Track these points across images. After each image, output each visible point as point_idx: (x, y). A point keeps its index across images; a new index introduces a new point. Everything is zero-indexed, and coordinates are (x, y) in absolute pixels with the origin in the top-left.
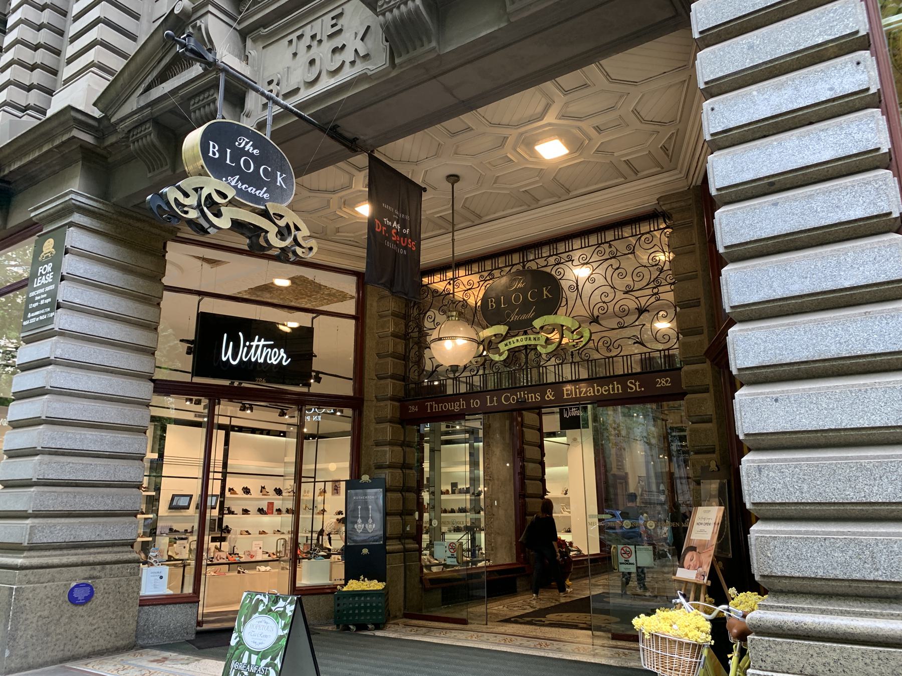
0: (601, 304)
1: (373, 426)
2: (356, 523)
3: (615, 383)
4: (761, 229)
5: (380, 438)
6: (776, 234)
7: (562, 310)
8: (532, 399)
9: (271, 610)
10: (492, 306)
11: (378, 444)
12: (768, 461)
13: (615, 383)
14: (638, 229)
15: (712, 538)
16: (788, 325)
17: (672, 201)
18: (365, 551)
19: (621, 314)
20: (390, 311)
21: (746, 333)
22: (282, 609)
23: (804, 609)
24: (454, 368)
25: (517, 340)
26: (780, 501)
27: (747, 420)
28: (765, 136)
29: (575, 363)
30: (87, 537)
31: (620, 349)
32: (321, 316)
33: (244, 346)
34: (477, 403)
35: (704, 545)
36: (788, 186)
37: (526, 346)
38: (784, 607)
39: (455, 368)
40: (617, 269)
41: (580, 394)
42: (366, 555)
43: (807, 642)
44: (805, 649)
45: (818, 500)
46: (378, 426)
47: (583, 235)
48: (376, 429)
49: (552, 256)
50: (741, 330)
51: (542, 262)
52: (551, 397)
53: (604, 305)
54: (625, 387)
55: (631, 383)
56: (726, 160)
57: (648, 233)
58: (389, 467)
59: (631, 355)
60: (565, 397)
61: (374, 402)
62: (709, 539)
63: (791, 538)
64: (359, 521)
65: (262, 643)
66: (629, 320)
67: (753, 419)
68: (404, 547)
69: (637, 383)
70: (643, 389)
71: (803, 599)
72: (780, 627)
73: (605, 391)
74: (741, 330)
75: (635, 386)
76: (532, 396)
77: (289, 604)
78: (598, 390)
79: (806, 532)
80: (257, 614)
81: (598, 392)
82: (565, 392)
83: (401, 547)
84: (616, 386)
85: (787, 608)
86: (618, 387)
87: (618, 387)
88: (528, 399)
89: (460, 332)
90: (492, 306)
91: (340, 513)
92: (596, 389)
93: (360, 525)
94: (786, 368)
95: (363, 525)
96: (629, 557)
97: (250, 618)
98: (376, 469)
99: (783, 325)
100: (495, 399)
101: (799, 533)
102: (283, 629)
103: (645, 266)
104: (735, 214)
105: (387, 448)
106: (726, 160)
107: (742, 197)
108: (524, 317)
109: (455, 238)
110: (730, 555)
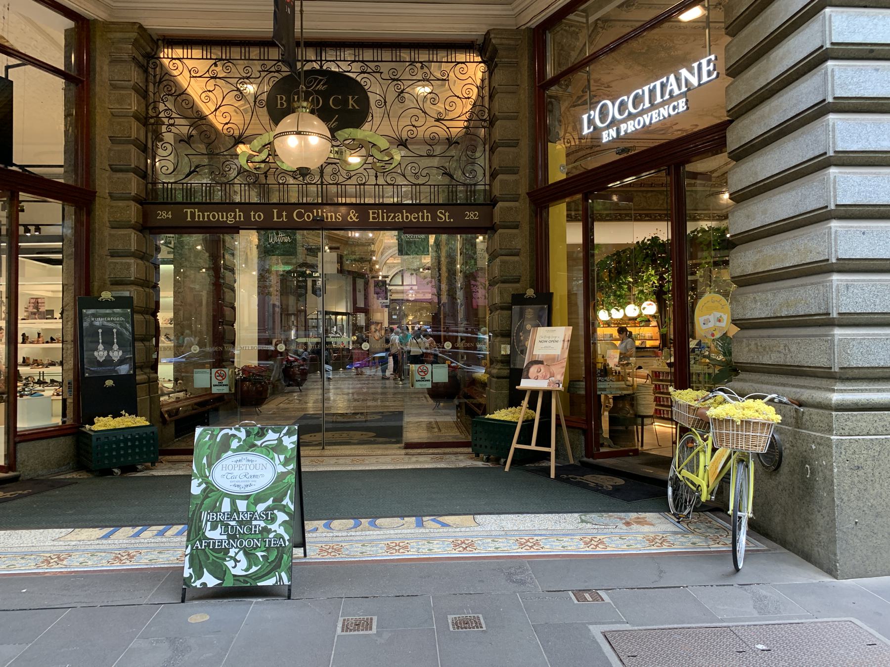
0: (412, 128)
1: (107, 232)
2: (96, 349)
3: (425, 211)
4: (865, 89)
5: (120, 247)
6: (875, 95)
7: (367, 126)
9: (255, 445)
10: (282, 104)
11: (114, 254)
12: (852, 281)
13: (425, 211)
15: (562, 352)
16: (875, 174)
17: (503, 36)
18: (109, 383)
19: (431, 142)
20: (132, 83)
21: (846, 175)
23: (866, 390)
24: (303, 172)
26: (860, 311)
27: (841, 248)
28: (865, 7)
29: (379, 185)
31: (428, 177)
32: (29, 68)
34: (259, 216)
35: (553, 359)
36: (881, 57)
38: (854, 390)
39: (305, 172)
40: (209, 91)
41: (387, 219)
42: (111, 388)
43: (873, 412)
44: (871, 417)
45: (885, 311)
46: (113, 232)
47: (224, 45)
48: (110, 235)
49: (357, 61)
50: (840, 173)
51: (344, 67)
52: (354, 219)
53: (414, 129)
54: (435, 216)
55: (441, 213)
56: (842, 18)
57: (333, 61)
58: (132, 283)
60: (371, 220)
61: (109, 200)
62: (559, 353)
63: (865, 339)
64: (101, 347)
65: (251, 485)
66: (438, 150)
67: (846, 247)
68: (149, 377)
69: (447, 214)
70: (452, 220)
71: (861, 383)
72: (856, 404)
73: (415, 218)
74: (840, 173)
77: (285, 435)
78: (407, 217)
79: (874, 335)
80: (230, 453)
82: (371, 216)
83: (145, 377)
84: (425, 215)
85: (856, 390)
86: (428, 216)
87: (428, 216)
89: (313, 125)
90: (282, 104)
91: (617, 309)
92: (405, 215)
93: (101, 353)
94: (870, 208)
95: (106, 353)
96: (426, 374)
98: (112, 284)
99: (871, 173)
100: (284, 213)
101: (869, 335)
102: (285, 464)
103: (458, 97)
104: (845, 69)
105: (131, 261)
106: (842, 18)
107: (846, 56)
109: (304, 9)
110: (672, 360)
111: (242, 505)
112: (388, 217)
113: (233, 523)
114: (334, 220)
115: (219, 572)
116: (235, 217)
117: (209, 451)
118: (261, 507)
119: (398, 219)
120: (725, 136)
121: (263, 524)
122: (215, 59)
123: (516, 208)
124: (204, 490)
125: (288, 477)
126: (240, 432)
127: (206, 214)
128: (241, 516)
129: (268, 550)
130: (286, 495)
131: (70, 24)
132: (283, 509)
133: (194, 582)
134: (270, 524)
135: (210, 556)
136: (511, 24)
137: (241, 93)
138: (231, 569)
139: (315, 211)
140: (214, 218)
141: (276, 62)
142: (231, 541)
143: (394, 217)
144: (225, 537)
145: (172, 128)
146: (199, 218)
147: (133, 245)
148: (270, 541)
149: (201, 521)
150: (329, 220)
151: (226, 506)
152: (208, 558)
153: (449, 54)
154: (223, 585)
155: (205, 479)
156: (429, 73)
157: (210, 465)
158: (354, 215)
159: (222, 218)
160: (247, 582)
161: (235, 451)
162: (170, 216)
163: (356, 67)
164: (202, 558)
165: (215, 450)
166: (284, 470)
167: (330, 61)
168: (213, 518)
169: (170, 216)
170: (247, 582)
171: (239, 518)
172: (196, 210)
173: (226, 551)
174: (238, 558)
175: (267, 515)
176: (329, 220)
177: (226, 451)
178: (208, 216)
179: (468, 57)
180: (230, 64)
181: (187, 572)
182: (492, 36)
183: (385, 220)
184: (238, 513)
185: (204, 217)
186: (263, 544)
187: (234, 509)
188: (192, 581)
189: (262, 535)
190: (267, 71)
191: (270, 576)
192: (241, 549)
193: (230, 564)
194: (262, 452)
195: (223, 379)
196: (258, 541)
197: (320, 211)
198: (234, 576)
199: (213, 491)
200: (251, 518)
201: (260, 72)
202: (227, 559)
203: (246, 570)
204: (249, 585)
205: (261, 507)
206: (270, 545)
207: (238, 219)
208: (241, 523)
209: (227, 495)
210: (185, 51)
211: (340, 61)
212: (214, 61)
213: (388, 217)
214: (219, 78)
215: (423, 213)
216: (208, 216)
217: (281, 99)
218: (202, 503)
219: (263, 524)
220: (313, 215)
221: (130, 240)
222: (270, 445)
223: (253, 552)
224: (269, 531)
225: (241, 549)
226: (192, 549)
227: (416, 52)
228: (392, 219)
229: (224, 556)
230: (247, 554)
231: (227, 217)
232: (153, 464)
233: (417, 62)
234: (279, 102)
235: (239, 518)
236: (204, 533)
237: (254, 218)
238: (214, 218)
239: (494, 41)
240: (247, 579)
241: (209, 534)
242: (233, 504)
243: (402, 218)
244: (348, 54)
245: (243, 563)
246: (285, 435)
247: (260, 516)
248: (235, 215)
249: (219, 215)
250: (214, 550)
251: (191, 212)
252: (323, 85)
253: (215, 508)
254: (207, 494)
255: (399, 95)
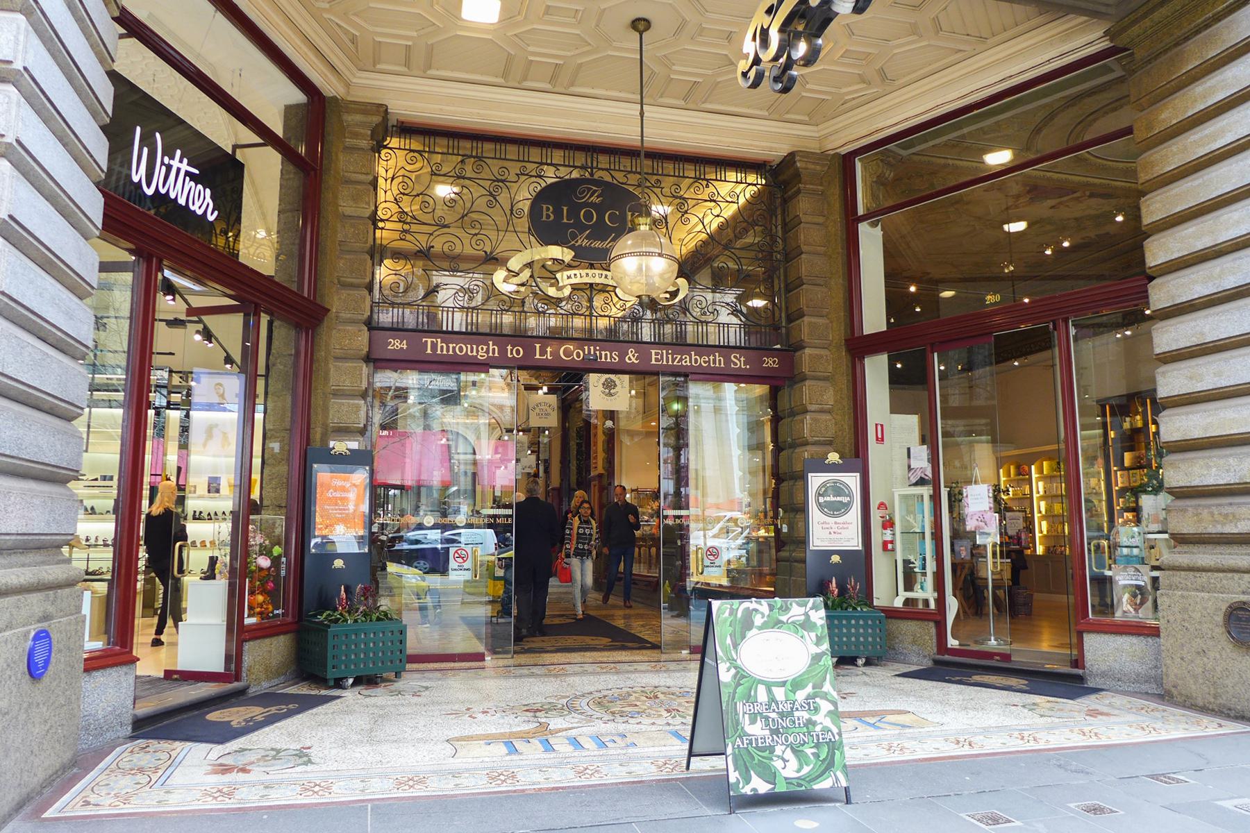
3: (717, 354)
8: (606, 358)
10: (548, 216)
13: (717, 354)
14: (723, 175)
22: (803, 618)
25: (587, 274)
30: (1240, 479)
33: (162, 163)
37: (591, 285)
41: (673, 362)
49: (634, 173)
51: (620, 176)
52: (634, 360)
54: (728, 361)
55: (735, 357)
57: (607, 170)
59: (728, 324)
60: (653, 362)
69: (742, 359)
70: (748, 367)
73: (705, 362)
75: (740, 361)
76: (606, 355)
77: (811, 609)
78: (696, 361)
80: (754, 631)
81: (696, 362)
82: (654, 357)
84: (717, 359)
88: (601, 358)
90: (548, 216)
92: (693, 358)
97: (743, 637)
102: (818, 643)
108: (597, 244)
111: (779, 693)
112: (673, 360)
113: (774, 715)
114: (609, 360)
115: (770, 777)
116: (487, 352)
117: (731, 629)
118: (801, 695)
119: (686, 362)
120: (1147, 291)
121: (806, 715)
122: (463, 156)
123: (827, 356)
124: (735, 676)
125: (824, 658)
126: (762, 605)
127: (451, 346)
128: (781, 706)
129: (817, 746)
130: (825, 679)
131: (297, 96)
132: (825, 696)
133: (743, 788)
134: (814, 715)
135: (755, 755)
136: (814, 147)
137: (495, 199)
138: (781, 770)
139: (586, 348)
140: (461, 351)
141: (537, 165)
142: (774, 736)
143: (681, 360)
144: (767, 732)
145: (407, 235)
146: (442, 351)
147: (363, 383)
148: (818, 736)
149: (737, 714)
150: (603, 360)
151: (762, 695)
152: (753, 758)
153: (718, 170)
154: (776, 790)
155: (732, 661)
156: (716, 193)
157: (735, 646)
158: (634, 356)
159: (472, 352)
160: (802, 786)
161: (760, 628)
162: (405, 347)
163: (633, 179)
164: (747, 758)
165: (738, 629)
166: (818, 651)
167: (603, 169)
168: (750, 710)
169: (405, 347)
170: (802, 786)
171: (778, 709)
172: (439, 340)
173: (771, 749)
174: (785, 756)
175: (809, 704)
176: (603, 360)
177: (750, 629)
178: (454, 348)
179: (402, 143)
180: (483, 164)
181: (733, 776)
182: (797, 158)
183: (670, 363)
184: (777, 703)
185: (448, 350)
186: (811, 738)
187: (772, 700)
188: (741, 786)
189: (808, 728)
190: (527, 175)
191: (824, 776)
192: (788, 746)
193: (778, 764)
194: (789, 629)
195: (465, 561)
196: (805, 735)
197: (592, 348)
198: (786, 779)
199: (744, 677)
200: (792, 708)
201: (517, 175)
202: (775, 758)
203: (798, 771)
204: (803, 788)
205: (801, 695)
206: (818, 740)
207: (491, 354)
208: (782, 715)
209: (761, 682)
210: (402, 140)
211: (615, 170)
212: (460, 158)
213: (673, 360)
214: (466, 178)
215: (715, 356)
216: (454, 348)
217: (548, 209)
218: (735, 692)
219: (806, 715)
220: (584, 353)
221: (361, 374)
222: (798, 621)
223: (801, 748)
224: (814, 724)
225: (788, 746)
226: (733, 748)
227: (432, 140)
228: (678, 362)
229: (770, 755)
230: (794, 751)
231: (478, 351)
232: (398, 675)
233: (703, 180)
234: (544, 214)
235: (778, 709)
236: (743, 728)
237: (512, 353)
238: (461, 351)
239: (798, 164)
240: (800, 782)
241: (750, 729)
242: (769, 691)
243: (691, 362)
244: (626, 163)
245: (793, 763)
246: (811, 609)
247: (802, 706)
248: (488, 349)
249: (467, 348)
250: (757, 748)
251: (432, 342)
252: (598, 197)
253: (749, 698)
254: (739, 680)
255: (683, 215)
